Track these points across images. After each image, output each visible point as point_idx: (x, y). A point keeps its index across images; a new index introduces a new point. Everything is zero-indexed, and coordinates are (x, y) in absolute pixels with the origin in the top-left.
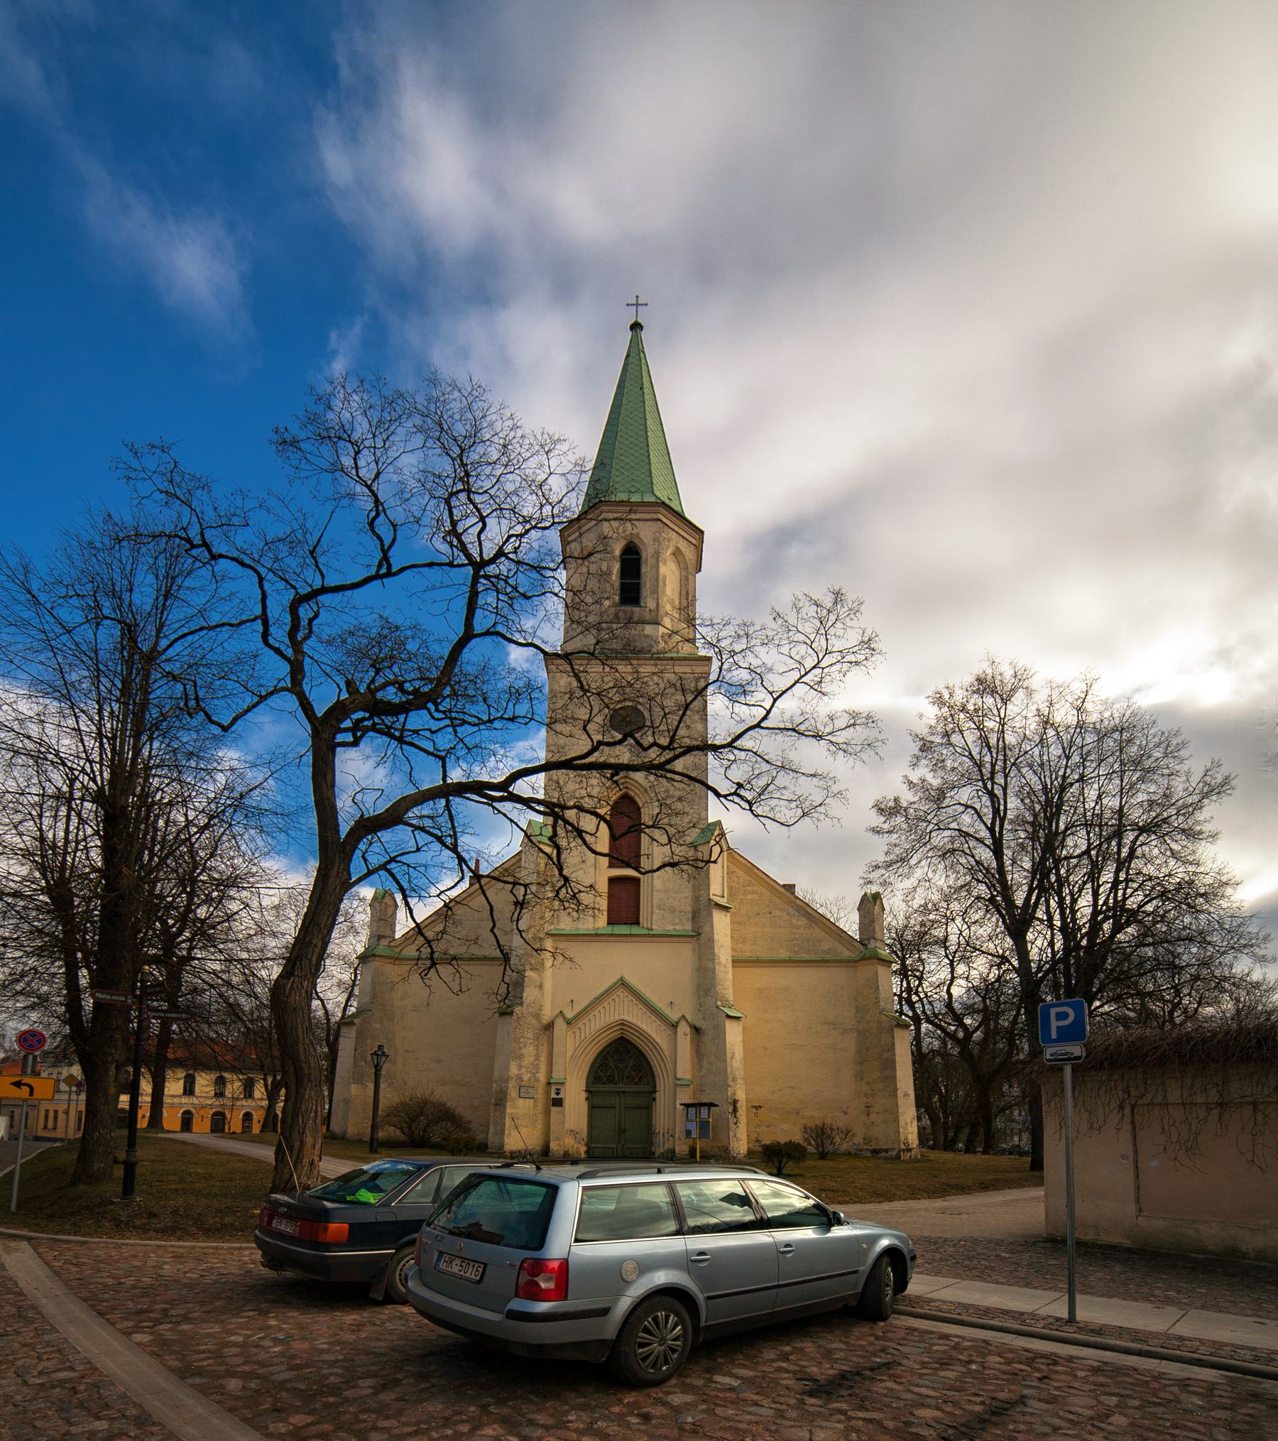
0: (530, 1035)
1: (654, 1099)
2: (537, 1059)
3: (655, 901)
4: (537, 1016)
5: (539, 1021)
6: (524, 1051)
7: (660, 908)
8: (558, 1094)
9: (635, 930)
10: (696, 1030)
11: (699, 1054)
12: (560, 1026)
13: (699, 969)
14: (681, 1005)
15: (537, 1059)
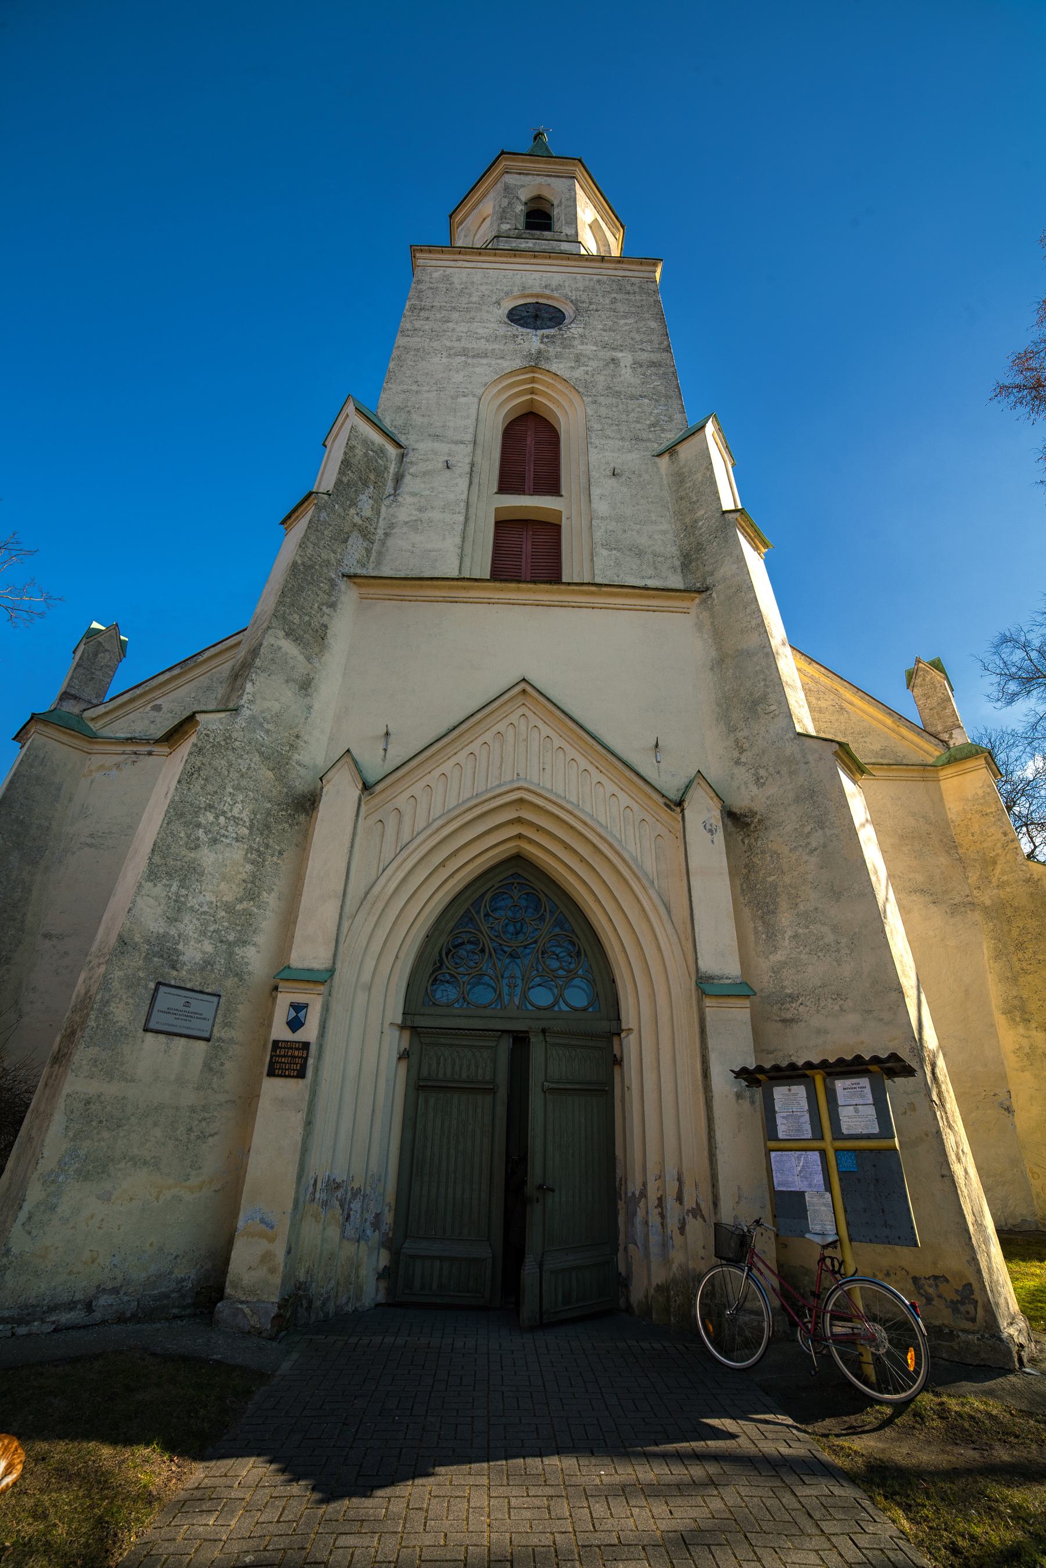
0: (242, 810)
1: (618, 1061)
2: (251, 894)
3: (598, 535)
4: (279, 761)
5: (280, 779)
6: (207, 857)
7: (606, 545)
8: (295, 1024)
9: (313, 1049)
10: (736, 820)
11: (754, 892)
12: (340, 797)
13: (719, 662)
14: (695, 747)
15: (251, 894)
